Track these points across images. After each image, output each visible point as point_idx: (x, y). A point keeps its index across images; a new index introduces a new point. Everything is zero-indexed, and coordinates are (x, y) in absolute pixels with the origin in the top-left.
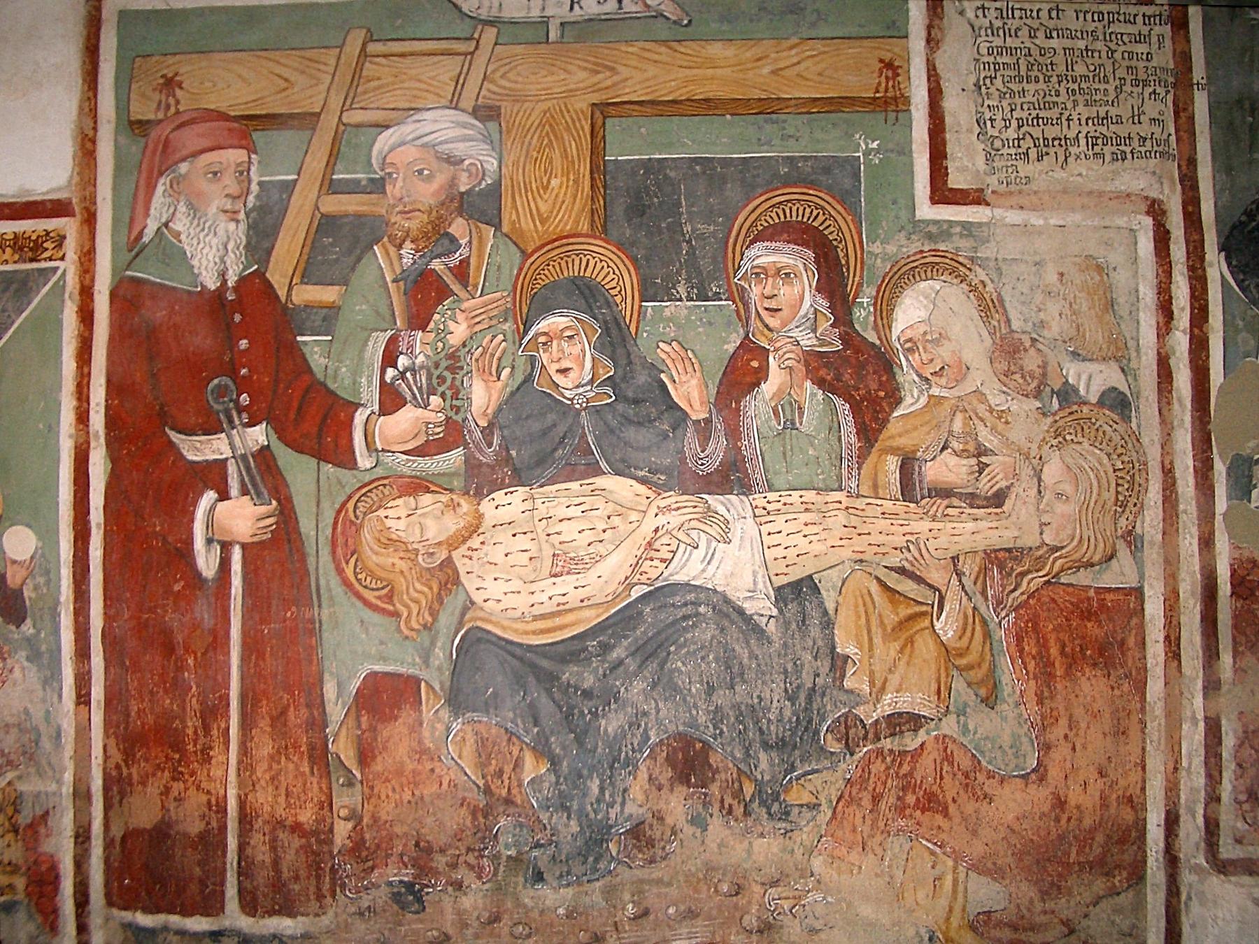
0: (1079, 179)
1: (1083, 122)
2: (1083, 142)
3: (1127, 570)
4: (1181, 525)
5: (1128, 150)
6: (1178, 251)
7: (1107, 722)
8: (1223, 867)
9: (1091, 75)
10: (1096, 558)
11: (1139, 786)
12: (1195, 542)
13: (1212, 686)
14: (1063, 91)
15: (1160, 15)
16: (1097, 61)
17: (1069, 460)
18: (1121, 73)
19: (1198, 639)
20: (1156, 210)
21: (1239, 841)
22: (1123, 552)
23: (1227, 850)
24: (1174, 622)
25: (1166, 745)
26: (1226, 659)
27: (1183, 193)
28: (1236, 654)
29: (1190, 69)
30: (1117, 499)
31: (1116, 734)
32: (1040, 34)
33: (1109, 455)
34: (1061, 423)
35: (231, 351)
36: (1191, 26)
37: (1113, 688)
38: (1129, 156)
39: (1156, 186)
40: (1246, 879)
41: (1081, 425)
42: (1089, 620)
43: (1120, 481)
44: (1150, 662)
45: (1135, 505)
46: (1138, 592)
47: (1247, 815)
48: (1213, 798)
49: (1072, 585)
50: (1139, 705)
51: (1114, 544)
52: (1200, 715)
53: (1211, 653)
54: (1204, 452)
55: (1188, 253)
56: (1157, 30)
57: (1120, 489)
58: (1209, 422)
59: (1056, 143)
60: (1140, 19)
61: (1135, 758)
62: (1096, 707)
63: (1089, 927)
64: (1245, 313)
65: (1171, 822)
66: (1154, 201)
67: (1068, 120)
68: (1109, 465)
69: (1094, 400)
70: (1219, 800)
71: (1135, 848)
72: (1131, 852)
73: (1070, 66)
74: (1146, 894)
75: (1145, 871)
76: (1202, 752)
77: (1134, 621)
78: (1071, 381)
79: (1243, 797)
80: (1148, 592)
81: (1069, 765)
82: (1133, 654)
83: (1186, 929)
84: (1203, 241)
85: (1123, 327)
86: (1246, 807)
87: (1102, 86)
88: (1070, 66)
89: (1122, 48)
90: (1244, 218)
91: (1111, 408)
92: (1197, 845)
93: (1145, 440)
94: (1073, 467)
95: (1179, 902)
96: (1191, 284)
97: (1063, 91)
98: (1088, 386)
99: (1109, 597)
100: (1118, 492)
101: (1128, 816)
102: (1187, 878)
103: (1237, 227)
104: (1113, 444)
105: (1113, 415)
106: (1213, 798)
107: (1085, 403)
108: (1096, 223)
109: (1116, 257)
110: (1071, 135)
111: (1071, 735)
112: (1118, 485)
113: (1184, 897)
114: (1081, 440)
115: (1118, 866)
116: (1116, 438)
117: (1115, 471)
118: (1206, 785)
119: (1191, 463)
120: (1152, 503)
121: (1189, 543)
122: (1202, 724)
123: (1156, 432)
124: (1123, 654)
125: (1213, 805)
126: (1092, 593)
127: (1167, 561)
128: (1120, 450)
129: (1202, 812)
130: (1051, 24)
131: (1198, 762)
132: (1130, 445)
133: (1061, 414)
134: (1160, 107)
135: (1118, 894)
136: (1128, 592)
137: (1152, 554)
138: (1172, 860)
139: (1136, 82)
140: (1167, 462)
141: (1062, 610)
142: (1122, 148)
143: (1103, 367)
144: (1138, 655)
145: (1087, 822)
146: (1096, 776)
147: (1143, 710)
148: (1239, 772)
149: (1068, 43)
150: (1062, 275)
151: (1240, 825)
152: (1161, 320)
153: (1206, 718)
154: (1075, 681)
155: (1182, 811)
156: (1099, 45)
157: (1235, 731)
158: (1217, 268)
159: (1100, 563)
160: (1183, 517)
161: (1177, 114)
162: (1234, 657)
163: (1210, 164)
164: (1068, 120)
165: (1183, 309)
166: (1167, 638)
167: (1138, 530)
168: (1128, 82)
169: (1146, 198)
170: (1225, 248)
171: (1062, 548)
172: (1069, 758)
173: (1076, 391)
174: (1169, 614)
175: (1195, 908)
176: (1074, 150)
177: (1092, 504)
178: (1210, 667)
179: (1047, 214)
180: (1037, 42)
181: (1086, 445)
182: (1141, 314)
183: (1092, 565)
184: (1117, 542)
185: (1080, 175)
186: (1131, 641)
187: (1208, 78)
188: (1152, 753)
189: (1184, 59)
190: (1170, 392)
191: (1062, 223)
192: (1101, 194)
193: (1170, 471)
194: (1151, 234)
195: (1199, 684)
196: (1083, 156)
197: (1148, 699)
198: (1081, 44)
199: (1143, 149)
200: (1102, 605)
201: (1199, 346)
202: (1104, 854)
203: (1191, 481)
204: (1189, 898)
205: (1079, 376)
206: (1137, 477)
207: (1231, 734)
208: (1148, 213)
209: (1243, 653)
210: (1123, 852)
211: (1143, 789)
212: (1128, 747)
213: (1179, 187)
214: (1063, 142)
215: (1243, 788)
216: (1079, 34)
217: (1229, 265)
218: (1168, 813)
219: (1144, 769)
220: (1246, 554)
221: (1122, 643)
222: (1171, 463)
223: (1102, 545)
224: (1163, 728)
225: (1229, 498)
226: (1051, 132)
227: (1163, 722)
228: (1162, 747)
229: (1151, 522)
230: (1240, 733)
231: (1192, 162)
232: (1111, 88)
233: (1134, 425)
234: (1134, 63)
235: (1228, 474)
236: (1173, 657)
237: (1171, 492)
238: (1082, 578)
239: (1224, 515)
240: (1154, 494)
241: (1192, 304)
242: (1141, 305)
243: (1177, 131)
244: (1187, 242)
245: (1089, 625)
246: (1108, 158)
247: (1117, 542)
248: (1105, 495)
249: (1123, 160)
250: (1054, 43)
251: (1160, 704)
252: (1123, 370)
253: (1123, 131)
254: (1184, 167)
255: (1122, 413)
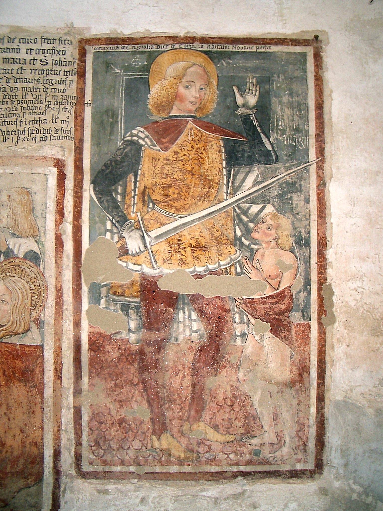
0: (23, 150)
1: (27, 123)
2: (26, 132)
3: (35, 337)
4: (64, 316)
5: (48, 135)
6: (70, 184)
7: (25, 407)
8: (84, 475)
9: (34, 100)
10: (20, 331)
11: (40, 437)
12: (72, 324)
13: (77, 392)
14: (19, 108)
15: (72, 71)
16: (38, 93)
17: (9, 285)
18: (49, 99)
19: (72, 370)
20: (60, 164)
21: (91, 464)
22: (34, 328)
23: (86, 468)
24: (59, 362)
25: (54, 419)
26: (85, 379)
27: (75, 156)
28: (90, 377)
29: (84, 96)
30: (32, 303)
31: (29, 413)
32: (11, 81)
33: (28, 282)
34: (4, 267)
35: (281, 86)
36: (87, 75)
37: (28, 392)
38: (49, 139)
39: (61, 153)
40: (95, 481)
41: (15, 267)
42: (17, 360)
43: (33, 295)
44: (46, 380)
45: (41, 306)
46: (41, 348)
47: (95, 452)
48: (79, 444)
49: (8, 343)
50: (40, 400)
51: (29, 324)
52: (72, 405)
53: (78, 376)
54: (78, 281)
55: (75, 185)
56: (70, 78)
57: (33, 298)
58: (80, 267)
59: (13, 133)
60: (62, 73)
61: (38, 424)
62: (20, 400)
63: (14, 503)
64: (100, 214)
65: (57, 454)
66: (59, 160)
67: (20, 122)
68: (28, 287)
69: (21, 255)
70: (81, 444)
71: (38, 466)
72: (36, 468)
73: (24, 96)
74: (42, 488)
75: (43, 477)
76: (72, 422)
77: (39, 361)
78: (10, 247)
79: (93, 444)
80: (46, 347)
81: (6, 427)
82: (37, 377)
83: (62, 503)
84: (82, 179)
85: (37, 221)
86: (94, 448)
87: (39, 105)
88: (24, 96)
89: (52, 87)
90: (104, 168)
91: (30, 260)
92: (71, 465)
93: (47, 275)
94: (10, 288)
95: (60, 492)
96: (74, 200)
97: (19, 108)
98: (19, 250)
99: (27, 349)
100: (32, 300)
101: (35, 451)
102: (64, 480)
103: (101, 172)
104: (29, 277)
105: (30, 263)
106: (79, 444)
107: (17, 258)
108: (28, 171)
109: (36, 188)
110: (21, 129)
111: (8, 412)
112: (32, 296)
113: (62, 489)
114: (14, 275)
115: (30, 474)
116: (32, 275)
117: (30, 290)
118: (75, 437)
119: (71, 286)
120: (50, 305)
121: (68, 325)
122: (72, 410)
123: (53, 271)
124: (33, 376)
125: (79, 447)
126: (18, 347)
127: (56, 333)
128: (33, 281)
129: (73, 450)
130: (17, 76)
131: (71, 426)
132: (39, 278)
133: (5, 263)
134: (67, 115)
135: (30, 487)
136: (36, 347)
137: (49, 331)
138: (57, 472)
139: (57, 103)
140: (59, 286)
141: (3, 355)
142: (46, 135)
143: (27, 240)
144: (40, 377)
145: (16, 453)
146: (19, 432)
147: (42, 402)
148: (91, 432)
149: (25, 85)
150: (10, 196)
151: (91, 456)
152: (58, 217)
153: (74, 407)
154: (10, 388)
155: (62, 449)
156: (40, 86)
157: (88, 413)
158: (88, 191)
159: (22, 333)
160: (65, 313)
161: (76, 118)
162: (89, 379)
163: (90, 142)
164: (20, 122)
165: (70, 212)
166: (55, 369)
167: (42, 318)
168: (53, 103)
169: (55, 159)
170: (94, 182)
171: (4, 326)
172: (7, 423)
173: (13, 252)
174: (56, 358)
175: (68, 495)
176: (22, 136)
177: (19, 306)
178: (77, 383)
179: (5, 168)
180: (9, 84)
181: (17, 278)
182: (47, 215)
183: (18, 334)
184: (31, 324)
185: (24, 148)
186: (37, 370)
187: (93, 100)
188: (47, 422)
189: (82, 91)
190: (62, 252)
191: (12, 172)
192: (32, 157)
193: (60, 290)
194: (56, 176)
195: (71, 391)
196: (26, 139)
197: (45, 397)
198: (31, 85)
199: (56, 135)
200: (23, 353)
201: (77, 230)
202: (24, 468)
203: (71, 294)
204: (65, 489)
205: (15, 244)
206: (42, 293)
207: (86, 415)
208: (55, 166)
209: (93, 377)
210: (33, 468)
211: (42, 439)
212: (35, 420)
213: (73, 153)
214: (17, 133)
215: (92, 440)
216: (30, 81)
217: (95, 190)
218: (55, 450)
219: (43, 429)
220: (97, 330)
221: (33, 371)
222: (61, 286)
223: (23, 325)
224: (52, 411)
225: (90, 303)
226: (11, 128)
227: (52, 408)
228: (52, 420)
229: (49, 314)
230: (91, 414)
231: (81, 141)
232: (43, 106)
233: (41, 268)
234: (56, 94)
235: (89, 292)
236: (58, 378)
237: (60, 300)
238: (14, 340)
239: (87, 311)
240: (51, 300)
241: (74, 209)
242: (48, 211)
243: (75, 126)
244: (75, 180)
245: (17, 362)
246: (38, 139)
247: (31, 324)
248: (26, 301)
249: (45, 141)
250: (17, 85)
251: (51, 400)
252: (36, 242)
253: (47, 126)
254: (77, 144)
255: (36, 262)
